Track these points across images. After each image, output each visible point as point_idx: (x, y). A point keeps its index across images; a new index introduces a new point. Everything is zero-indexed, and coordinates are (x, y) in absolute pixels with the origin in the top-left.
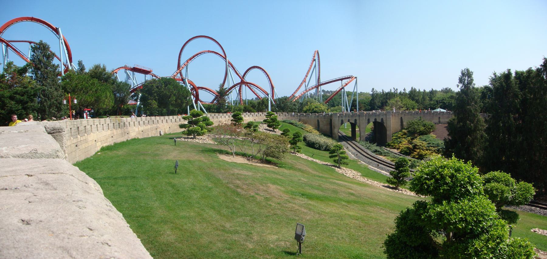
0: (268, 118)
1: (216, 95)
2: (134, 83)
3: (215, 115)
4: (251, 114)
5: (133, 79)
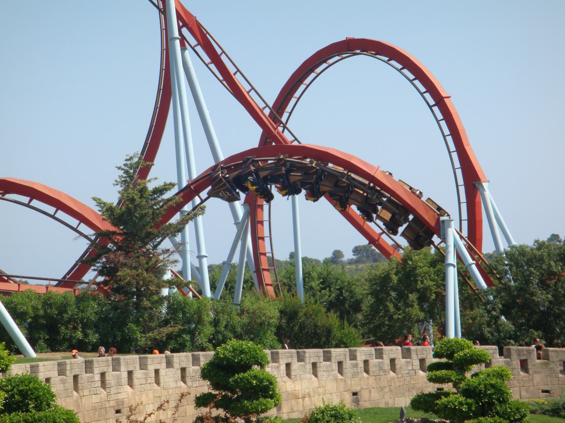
0: (448, 387)
1: (100, 234)
3: (89, 366)
4: (327, 358)
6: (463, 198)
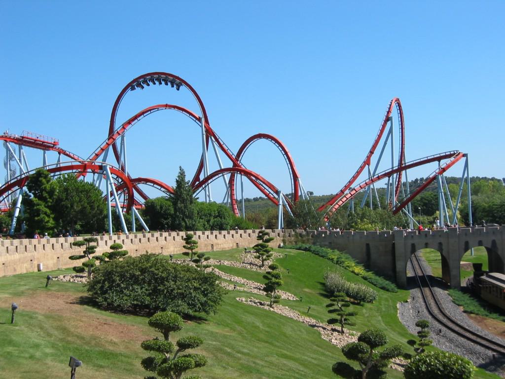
2: (20, 168)
5: (20, 160)
6: (293, 183)
